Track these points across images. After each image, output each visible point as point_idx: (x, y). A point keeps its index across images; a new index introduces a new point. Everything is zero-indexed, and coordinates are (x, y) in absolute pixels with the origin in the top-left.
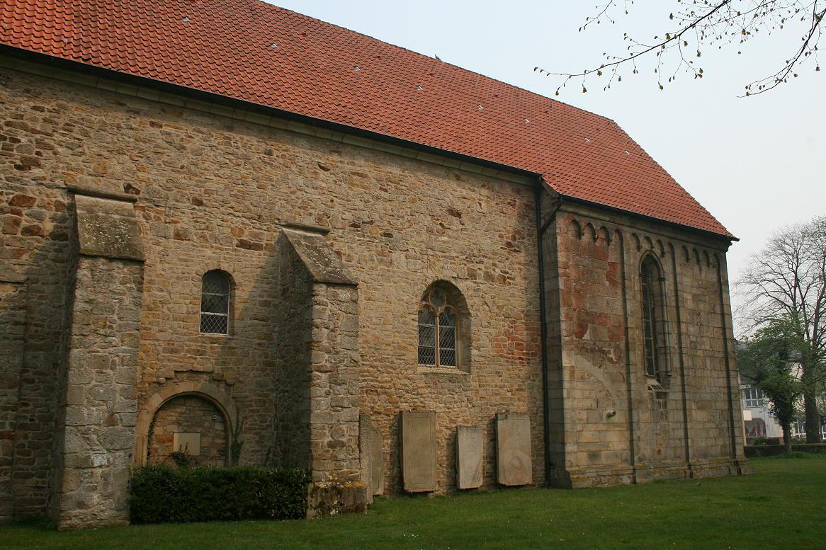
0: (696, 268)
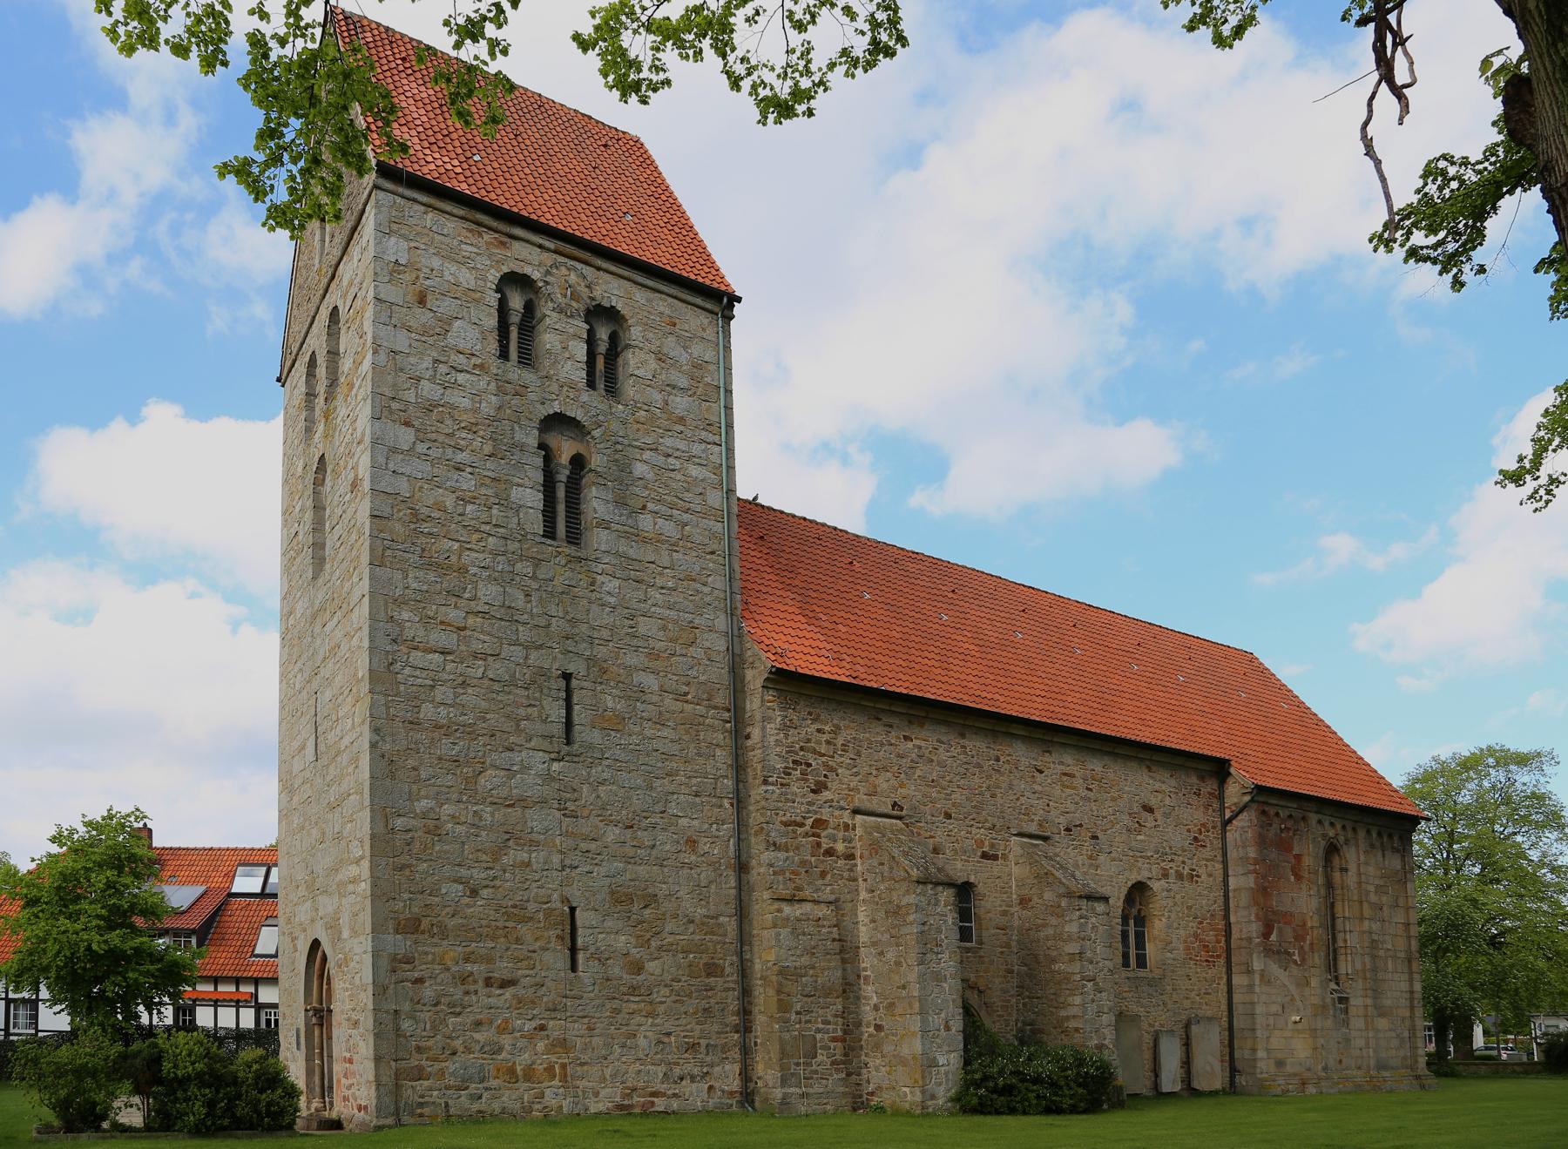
0: (1380, 854)
